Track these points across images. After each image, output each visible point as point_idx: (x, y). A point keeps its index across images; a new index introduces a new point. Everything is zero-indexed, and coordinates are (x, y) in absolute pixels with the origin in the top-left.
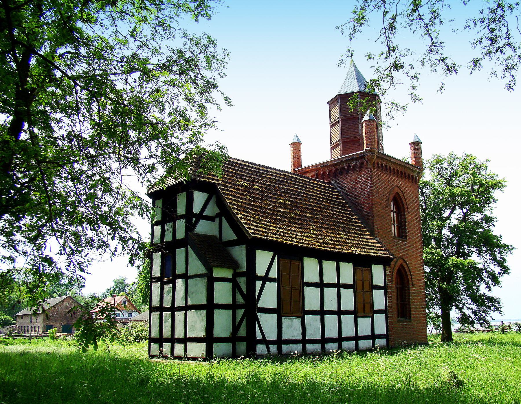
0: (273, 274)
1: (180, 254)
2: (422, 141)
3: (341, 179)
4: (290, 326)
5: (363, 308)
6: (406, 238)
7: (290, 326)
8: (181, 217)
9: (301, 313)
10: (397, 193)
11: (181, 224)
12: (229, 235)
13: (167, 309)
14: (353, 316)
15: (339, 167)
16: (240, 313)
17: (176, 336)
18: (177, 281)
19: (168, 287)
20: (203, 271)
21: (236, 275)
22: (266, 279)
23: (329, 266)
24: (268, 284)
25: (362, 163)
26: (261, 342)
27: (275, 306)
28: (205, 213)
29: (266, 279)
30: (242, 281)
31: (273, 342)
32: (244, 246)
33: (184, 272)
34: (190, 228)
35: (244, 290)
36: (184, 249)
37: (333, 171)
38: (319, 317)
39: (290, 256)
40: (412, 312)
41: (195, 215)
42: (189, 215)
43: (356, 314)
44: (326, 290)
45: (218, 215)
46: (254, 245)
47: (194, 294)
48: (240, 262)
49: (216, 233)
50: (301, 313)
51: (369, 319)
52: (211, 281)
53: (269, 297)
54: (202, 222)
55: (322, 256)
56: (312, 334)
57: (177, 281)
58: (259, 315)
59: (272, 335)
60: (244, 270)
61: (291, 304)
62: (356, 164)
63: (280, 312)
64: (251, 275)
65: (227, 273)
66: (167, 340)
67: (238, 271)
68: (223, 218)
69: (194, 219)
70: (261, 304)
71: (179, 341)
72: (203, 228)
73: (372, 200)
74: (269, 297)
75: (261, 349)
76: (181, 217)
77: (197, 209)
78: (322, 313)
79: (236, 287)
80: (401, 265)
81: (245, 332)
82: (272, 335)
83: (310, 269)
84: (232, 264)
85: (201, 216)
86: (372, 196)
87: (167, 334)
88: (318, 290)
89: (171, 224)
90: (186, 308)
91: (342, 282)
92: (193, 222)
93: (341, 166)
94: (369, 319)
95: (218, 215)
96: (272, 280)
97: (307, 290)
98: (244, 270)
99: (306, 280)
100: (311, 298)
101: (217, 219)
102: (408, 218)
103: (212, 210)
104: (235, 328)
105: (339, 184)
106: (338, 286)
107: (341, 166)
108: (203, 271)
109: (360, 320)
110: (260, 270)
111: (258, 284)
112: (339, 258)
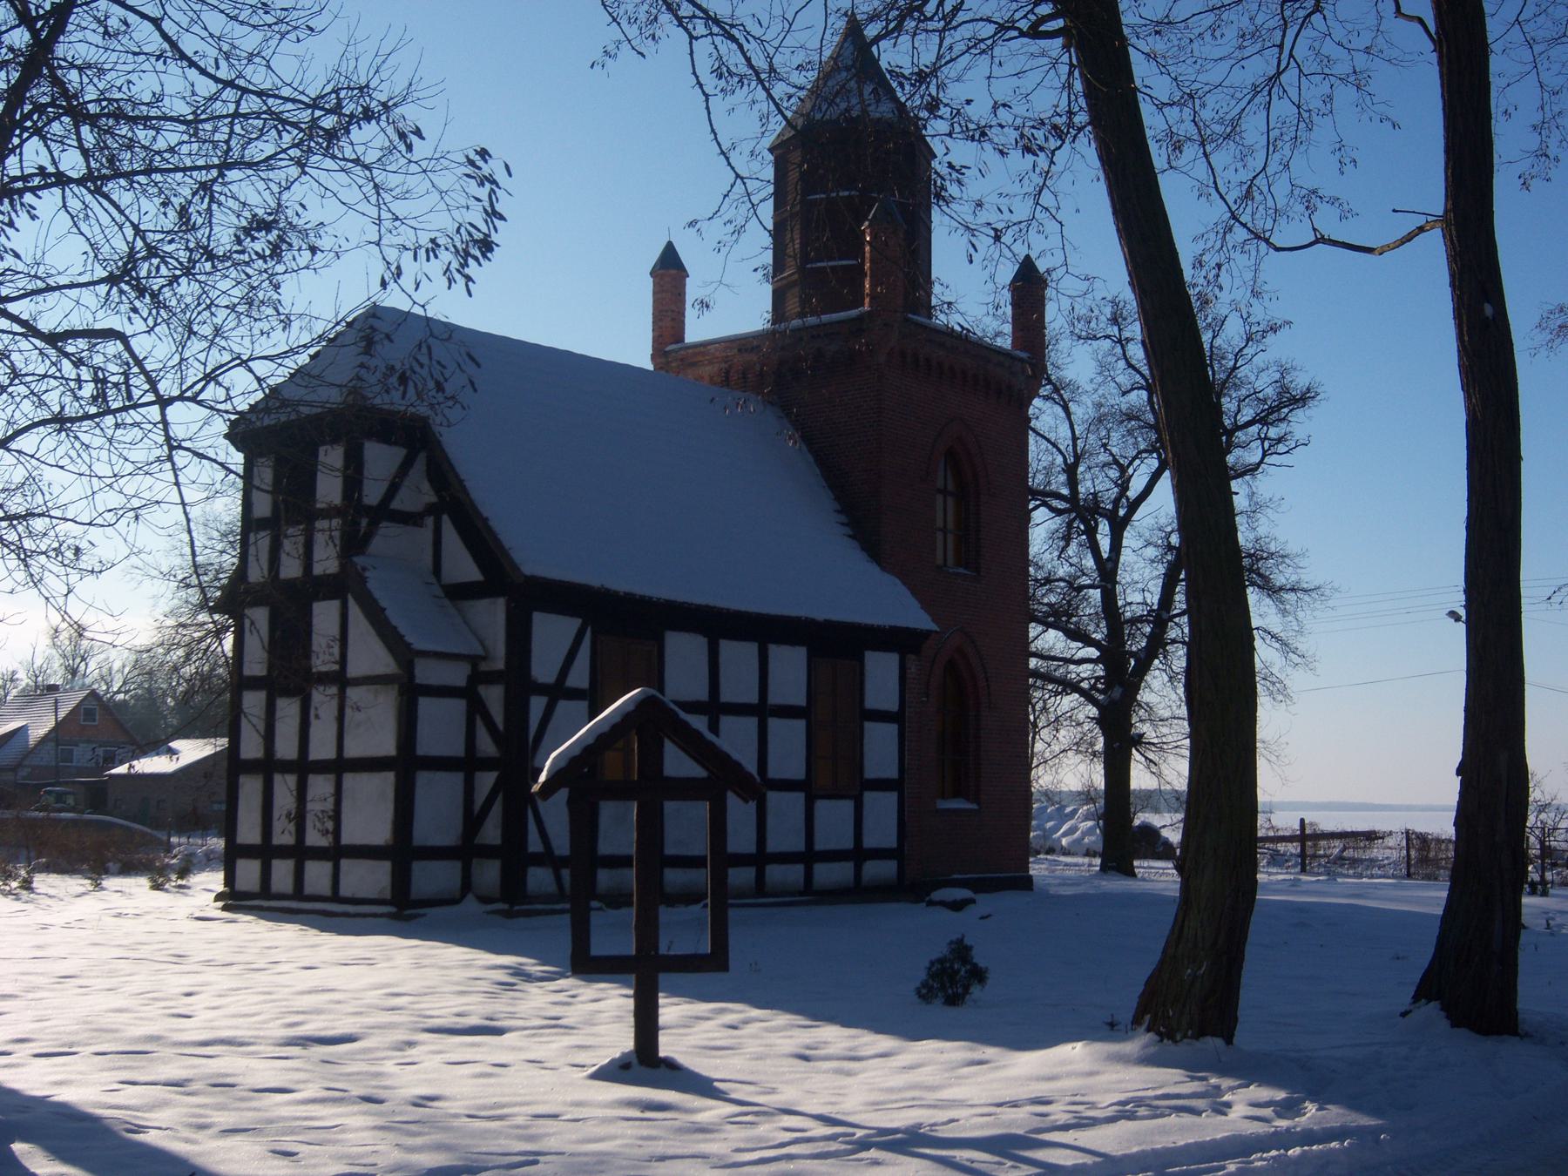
1: (325, 616)
19: (288, 709)
23: (739, 657)
28: (396, 505)
30: (494, 696)
35: (499, 719)
45: (433, 510)
51: (847, 806)
69: (364, 522)
77: (372, 494)
79: (476, 708)
85: (384, 512)
88: (752, 722)
94: (847, 806)
95: (431, 510)
101: (430, 521)
103: (417, 494)
104: (473, 821)
111: (537, 704)
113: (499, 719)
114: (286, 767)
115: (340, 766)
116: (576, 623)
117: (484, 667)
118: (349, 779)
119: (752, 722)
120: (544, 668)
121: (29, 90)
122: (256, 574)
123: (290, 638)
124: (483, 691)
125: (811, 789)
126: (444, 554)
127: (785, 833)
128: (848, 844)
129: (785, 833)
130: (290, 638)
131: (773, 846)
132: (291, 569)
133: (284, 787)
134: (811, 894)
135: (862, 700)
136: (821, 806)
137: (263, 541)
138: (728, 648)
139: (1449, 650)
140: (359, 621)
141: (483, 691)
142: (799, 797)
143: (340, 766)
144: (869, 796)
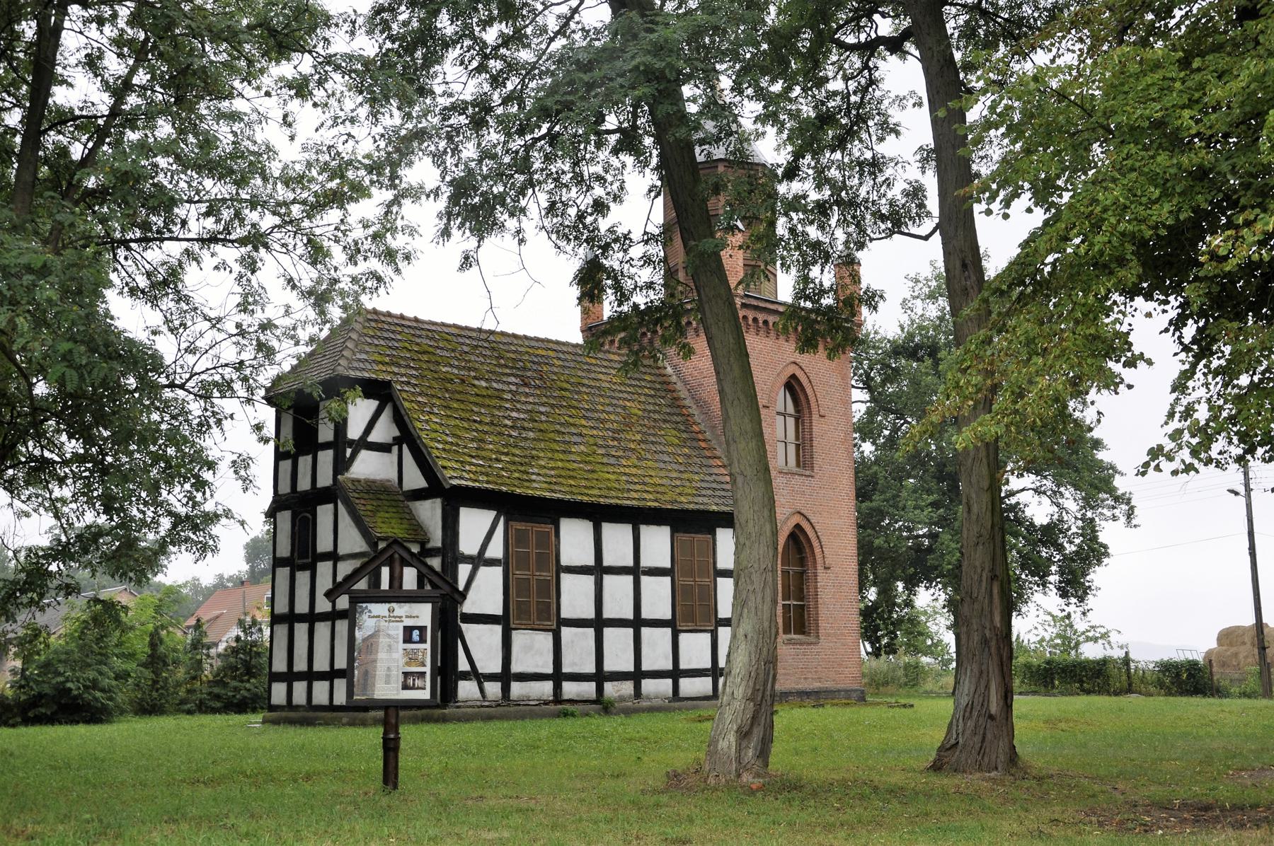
0: (496, 549)
1: (324, 513)
4: (528, 648)
5: (692, 611)
7: (528, 648)
8: (326, 446)
9: (555, 624)
11: (326, 457)
12: (414, 479)
14: (668, 631)
17: (317, 668)
18: (319, 564)
19: (303, 578)
20: (433, 509)
22: (479, 561)
23: (617, 540)
24: (483, 571)
26: (465, 676)
27: (499, 611)
28: (370, 439)
29: (479, 561)
31: (492, 677)
32: (438, 502)
33: (330, 548)
36: (331, 506)
38: (590, 632)
39: (530, 514)
40: (822, 624)
41: (351, 443)
43: (674, 625)
44: (608, 580)
45: (398, 441)
46: (456, 500)
48: (431, 529)
49: (393, 475)
50: (555, 624)
51: (706, 638)
53: (486, 592)
54: (364, 455)
55: (598, 514)
56: (574, 664)
57: (319, 564)
59: (490, 662)
60: (439, 544)
61: (531, 604)
63: (506, 622)
66: (300, 676)
67: (430, 546)
68: (405, 446)
69: (349, 451)
70: (470, 606)
71: (322, 676)
72: (368, 466)
74: (486, 592)
75: (467, 689)
76: (326, 446)
78: (599, 623)
80: (798, 526)
82: (490, 662)
83: (575, 541)
85: (364, 443)
87: (300, 665)
88: (629, 579)
89: (309, 458)
91: (646, 562)
92: (348, 455)
94: (706, 638)
96: (492, 562)
97: (567, 580)
98: (439, 544)
99: (565, 560)
100: (576, 596)
101: (395, 449)
102: (818, 427)
103: (384, 431)
108: (433, 509)
109: (683, 637)
110: (469, 543)
111: (464, 570)
112: (637, 517)
114: (301, 618)
116: (492, 514)
119: (629, 579)
121: (1000, 491)
122: (285, 488)
123: (304, 532)
125: (674, 625)
127: (619, 655)
128: (630, 668)
129: (619, 655)
130: (304, 532)
131: (609, 666)
132: (304, 484)
134: (602, 704)
135: (715, 563)
137: (286, 465)
138: (608, 530)
139: (1248, 558)
140: (345, 520)
142: (668, 631)
144: (566, 632)
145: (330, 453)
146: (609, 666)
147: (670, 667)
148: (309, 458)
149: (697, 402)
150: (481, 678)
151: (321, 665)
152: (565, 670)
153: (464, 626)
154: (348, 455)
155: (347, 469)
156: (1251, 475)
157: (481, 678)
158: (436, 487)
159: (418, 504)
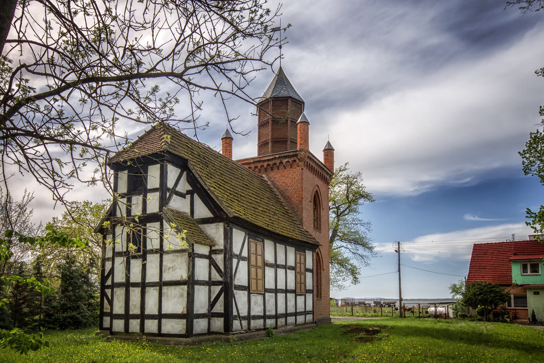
2: (334, 148)
3: (272, 174)
6: (320, 230)
8: (154, 190)
10: (317, 191)
13: (282, 291)
15: (271, 163)
16: (217, 289)
21: (212, 252)
25: (295, 161)
30: (219, 259)
31: (244, 318)
34: (164, 201)
35: (222, 267)
37: (265, 166)
42: (163, 189)
47: (171, 270)
51: (303, 297)
52: (192, 256)
58: (235, 291)
62: (288, 162)
64: (228, 252)
65: (205, 250)
68: (195, 195)
69: (168, 194)
70: (237, 282)
73: (302, 194)
75: (236, 324)
76: (154, 190)
77: (170, 184)
79: (213, 263)
81: (223, 308)
84: (210, 242)
86: (302, 190)
89: (141, 198)
90: (276, 291)
92: (168, 196)
93: (273, 162)
95: (188, 192)
98: (222, 247)
103: (184, 186)
104: (212, 305)
105: (269, 178)
106: (276, 266)
107: (273, 162)
111: (235, 261)
113: (222, 267)
115: (161, 284)
117: (213, 248)
118: (165, 289)
120: (236, 250)
124: (213, 256)
126: (189, 207)
133: (135, 293)
136: (298, 297)
141: (213, 256)
143: (161, 284)
145: (157, 194)
146: (147, 312)
147: (123, 313)
148: (141, 198)
149: (284, 197)
150: (241, 318)
151: (291, 310)
152: (131, 313)
153: (235, 291)
154: (168, 196)
155: (167, 204)
156: (400, 246)
157: (241, 318)
158: (218, 215)
159: (206, 226)
